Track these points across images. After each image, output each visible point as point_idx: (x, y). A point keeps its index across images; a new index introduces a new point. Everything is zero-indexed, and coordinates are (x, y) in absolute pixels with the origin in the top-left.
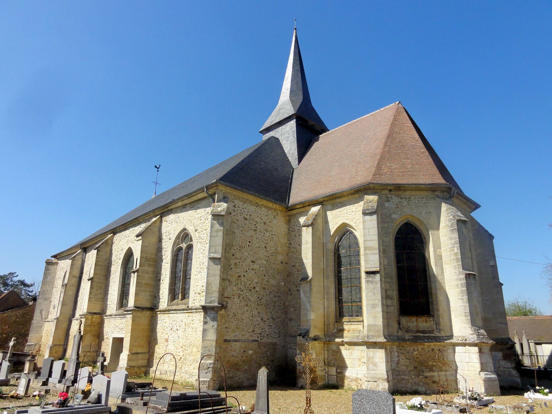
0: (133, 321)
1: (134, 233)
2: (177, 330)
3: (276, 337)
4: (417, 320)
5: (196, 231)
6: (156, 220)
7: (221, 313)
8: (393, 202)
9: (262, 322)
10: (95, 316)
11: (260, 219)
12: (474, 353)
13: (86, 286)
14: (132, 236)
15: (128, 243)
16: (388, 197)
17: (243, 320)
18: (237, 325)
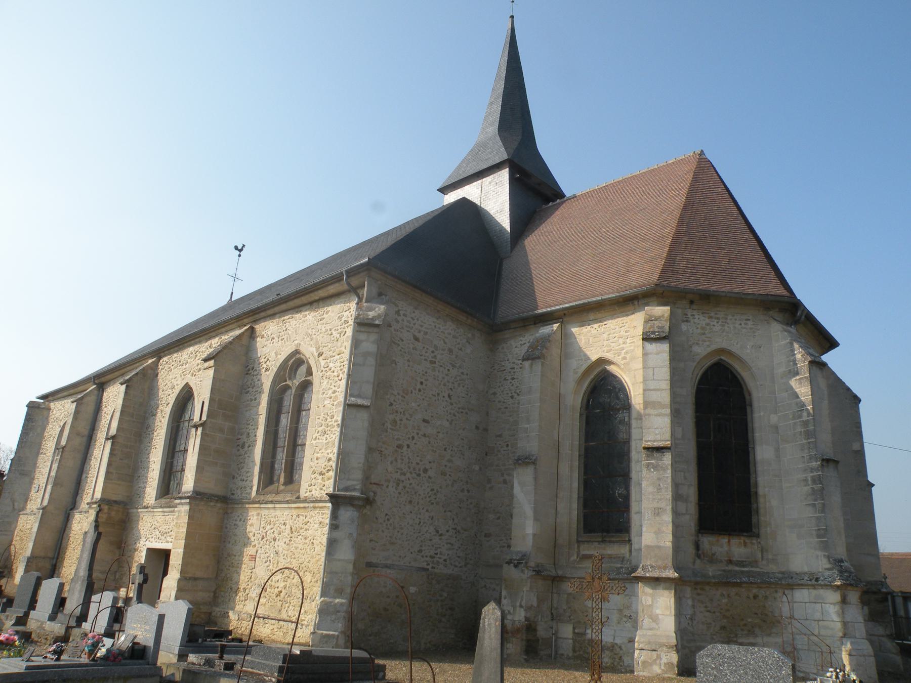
0: (191, 518)
1: (197, 358)
2: (275, 540)
3: (460, 565)
4: (729, 541)
5: (320, 355)
6: (243, 333)
7: (364, 512)
8: (695, 323)
9: (435, 535)
10: (116, 507)
11: (442, 342)
12: (831, 604)
13: (101, 454)
14: (194, 363)
15: (184, 375)
16: (687, 315)
17: (402, 529)
18: (391, 537)
